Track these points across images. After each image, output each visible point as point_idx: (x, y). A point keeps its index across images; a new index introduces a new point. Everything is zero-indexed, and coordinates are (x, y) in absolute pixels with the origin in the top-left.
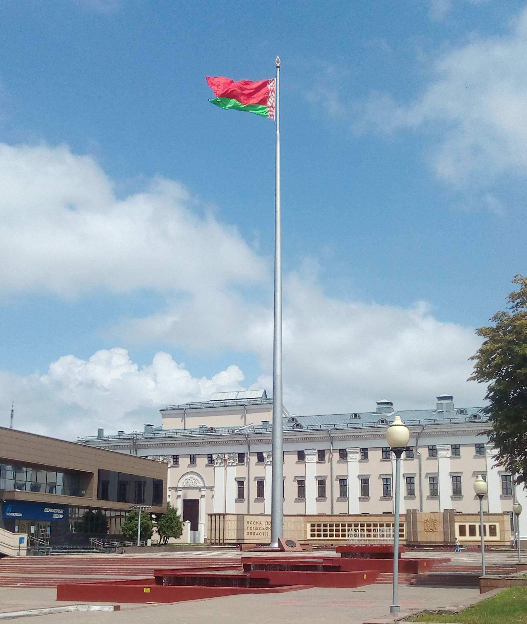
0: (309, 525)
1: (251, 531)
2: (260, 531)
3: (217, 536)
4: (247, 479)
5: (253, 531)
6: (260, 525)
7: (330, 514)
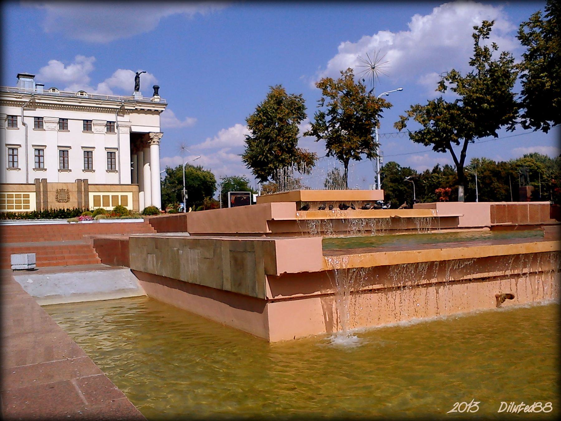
4: (23, 145)
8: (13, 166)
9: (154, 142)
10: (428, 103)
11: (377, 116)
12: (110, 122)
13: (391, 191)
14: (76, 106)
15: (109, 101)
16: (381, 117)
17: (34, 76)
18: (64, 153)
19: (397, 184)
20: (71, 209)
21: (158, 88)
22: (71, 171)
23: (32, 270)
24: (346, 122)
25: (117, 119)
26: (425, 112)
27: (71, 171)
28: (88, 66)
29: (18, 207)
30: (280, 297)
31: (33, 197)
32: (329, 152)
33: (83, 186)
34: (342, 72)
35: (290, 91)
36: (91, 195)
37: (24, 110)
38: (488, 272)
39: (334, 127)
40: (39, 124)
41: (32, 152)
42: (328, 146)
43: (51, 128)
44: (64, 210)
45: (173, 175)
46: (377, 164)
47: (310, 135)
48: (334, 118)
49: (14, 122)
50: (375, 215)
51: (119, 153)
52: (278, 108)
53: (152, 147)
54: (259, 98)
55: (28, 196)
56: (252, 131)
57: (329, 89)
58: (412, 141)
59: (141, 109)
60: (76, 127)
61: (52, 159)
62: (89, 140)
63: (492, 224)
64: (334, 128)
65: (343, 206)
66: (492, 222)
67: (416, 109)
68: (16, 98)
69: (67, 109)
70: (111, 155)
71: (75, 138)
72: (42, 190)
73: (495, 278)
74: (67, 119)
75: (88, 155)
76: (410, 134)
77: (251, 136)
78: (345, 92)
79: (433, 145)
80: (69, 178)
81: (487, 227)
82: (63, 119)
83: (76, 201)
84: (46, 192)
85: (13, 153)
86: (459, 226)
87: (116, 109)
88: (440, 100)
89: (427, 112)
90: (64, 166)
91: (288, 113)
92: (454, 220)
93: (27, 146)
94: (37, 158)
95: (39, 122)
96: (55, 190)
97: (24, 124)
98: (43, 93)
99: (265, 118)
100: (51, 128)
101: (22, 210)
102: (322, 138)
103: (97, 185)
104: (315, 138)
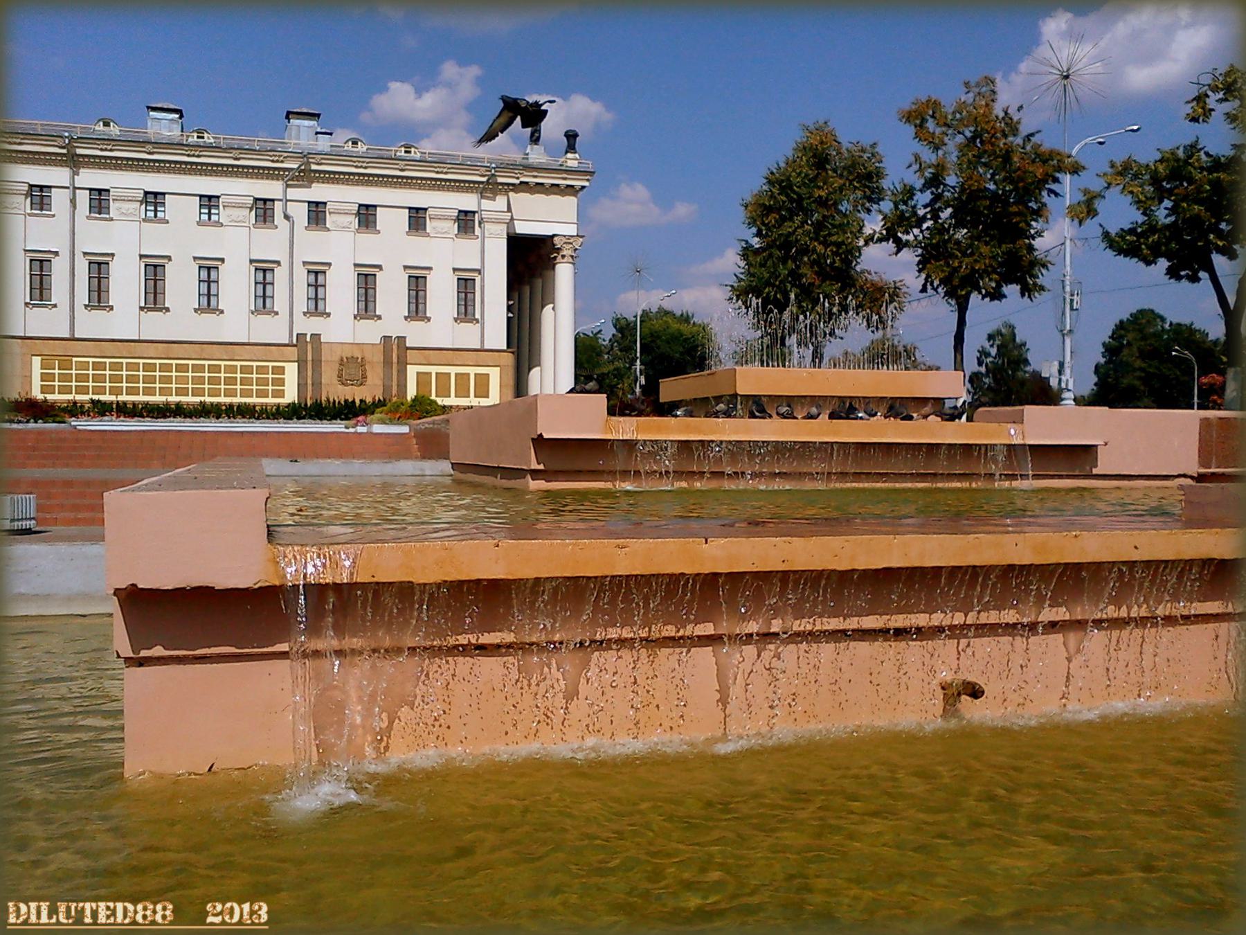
0: (37, 361)
7: (67, 336)
8: (264, 306)
9: (563, 256)
10: (1158, 156)
11: (1045, 193)
12: (466, 212)
13: (1139, 378)
14: (393, 177)
15: (462, 165)
16: (1056, 194)
17: (318, 115)
18: (367, 281)
19: (1155, 363)
20: (369, 400)
21: (576, 135)
22: (379, 318)
23: (28, 532)
24: (968, 206)
26: (1147, 177)
27: (379, 318)
29: (262, 394)
30: (158, 651)
31: (291, 371)
32: (926, 280)
33: (396, 352)
34: (967, 84)
35: (850, 135)
36: (412, 371)
37: (288, 186)
38: (999, 608)
39: (935, 217)
40: (367, 220)
41: (82, 267)
42: (923, 264)
43: (341, 222)
44: (354, 402)
45: (627, 333)
46: (1064, 313)
47: (880, 240)
48: (937, 197)
49: (46, 200)
50: (835, 434)
51: (483, 280)
52: (816, 177)
53: (558, 266)
54: (777, 148)
55: (281, 370)
56: (754, 230)
57: (931, 125)
58: (1110, 253)
59: (537, 184)
60: (392, 222)
61: (341, 291)
62: (419, 251)
63: (1203, 470)
64: (936, 222)
65: (898, 408)
66: (1202, 465)
67: (1126, 171)
68: (101, 150)
69: (376, 184)
70: (466, 286)
72: (310, 358)
73: (937, 631)
74: (164, 194)
75: (417, 283)
76: (1106, 235)
77: (756, 242)
78: (969, 134)
79: (1163, 264)
80: (370, 333)
81: (1185, 476)
82: (367, 206)
83: (380, 383)
84: (317, 362)
86: (1095, 471)
88: (1193, 149)
89: (1151, 178)
90: (366, 306)
91: (841, 189)
92: (1085, 453)
93: (292, 264)
94: (312, 289)
95: (100, 200)
96: (337, 358)
97: (287, 217)
98: (327, 149)
99: (784, 198)
100: (341, 222)
101: (270, 400)
102: (907, 244)
103: (231, 344)
104: (891, 246)
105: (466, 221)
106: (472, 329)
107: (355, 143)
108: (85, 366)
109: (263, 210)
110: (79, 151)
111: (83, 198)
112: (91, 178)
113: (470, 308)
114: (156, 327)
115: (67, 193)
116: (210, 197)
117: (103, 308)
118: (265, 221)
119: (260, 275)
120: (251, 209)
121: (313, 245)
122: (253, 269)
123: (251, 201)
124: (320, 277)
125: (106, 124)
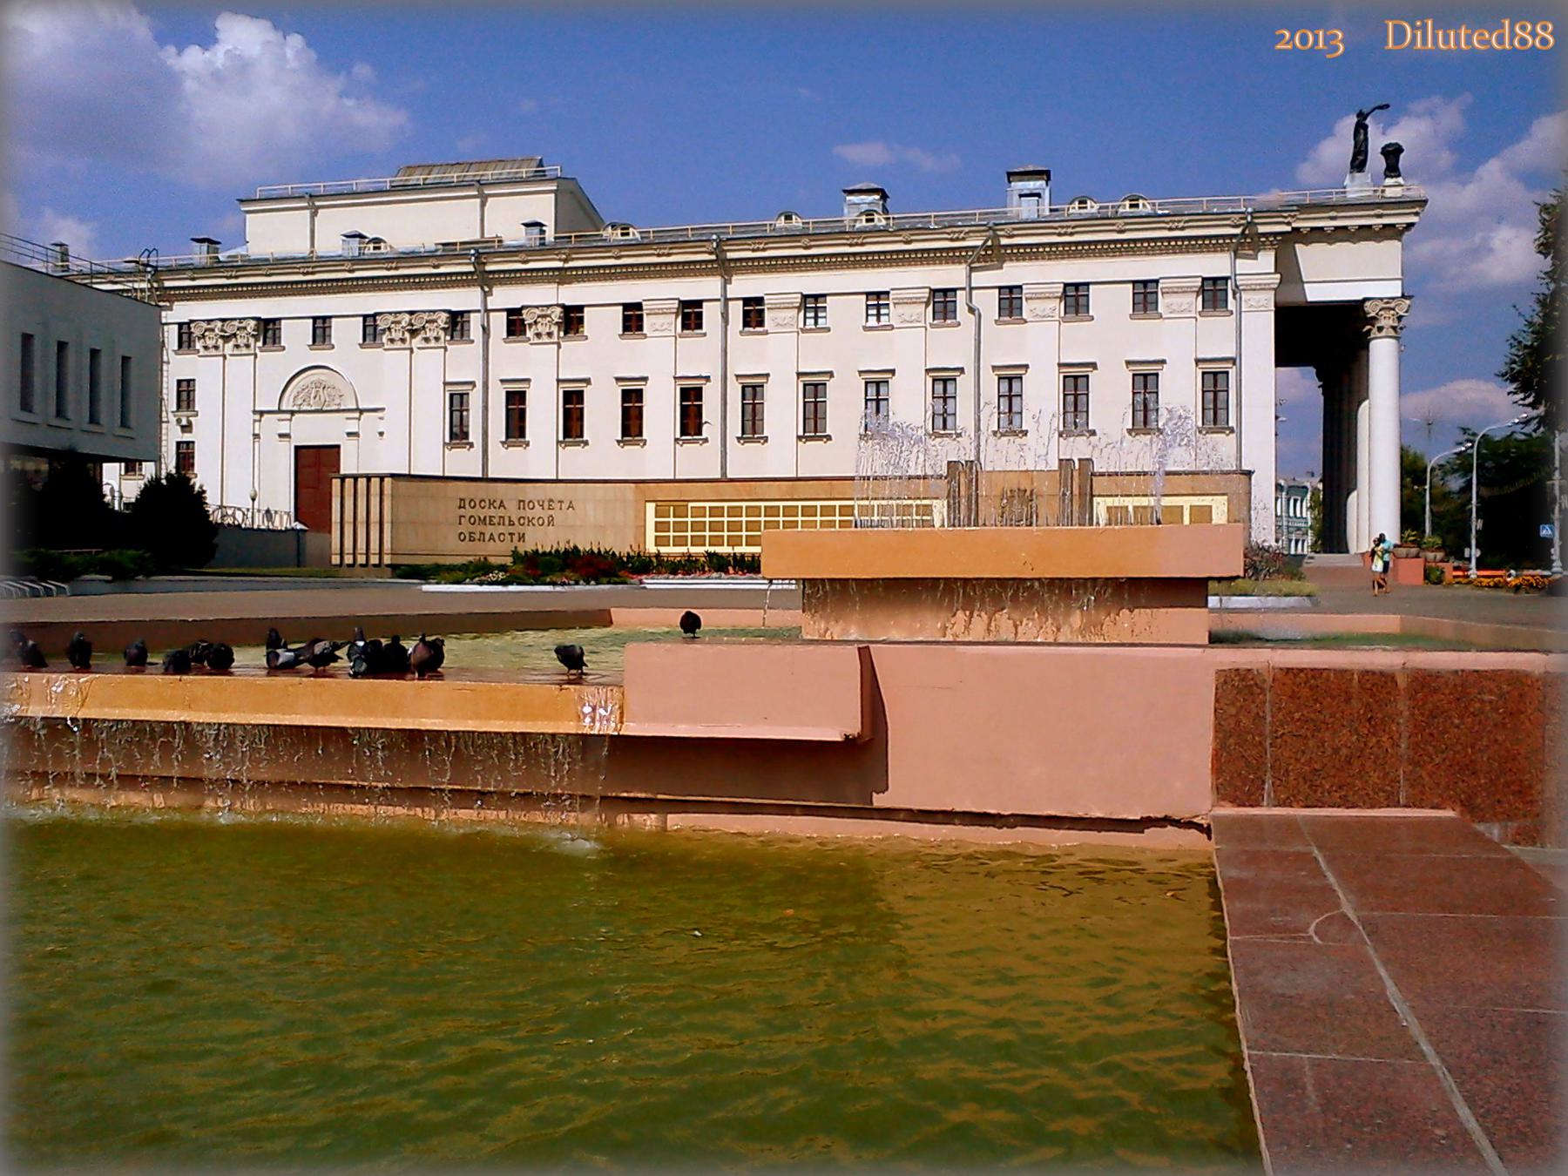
0: (651, 507)
1: (472, 528)
2: (501, 529)
3: (374, 546)
4: (479, 385)
5: (478, 528)
6: (501, 512)
7: (718, 476)
9: (1380, 329)
12: (1215, 280)
25: (1234, 267)
28: (1451, 118)
33: (1079, 482)
37: (972, 270)
43: (1042, 312)
53: (1374, 345)
55: (928, 510)
60: (603, 324)
71: (845, 346)
74: (1087, 284)
85: (945, 391)
87: (1231, 236)
97: (971, 310)
100: (1042, 312)
105: (1214, 293)
106: (1225, 442)
107: (788, 218)
108: (700, 512)
109: (942, 303)
110: (730, 255)
111: (736, 310)
112: (745, 285)
113: (1221, 413)
114: (819, 460)
115: (718, 306)
116: (878, 295)
117: (757, 440)
118: (1145, 310)
119: (1005, 384)
120: (927, 304)
121: (1005, 343)
122: (930, 381)
123: (676, 304)
124: (1015, 384)
125: (788, 218)
